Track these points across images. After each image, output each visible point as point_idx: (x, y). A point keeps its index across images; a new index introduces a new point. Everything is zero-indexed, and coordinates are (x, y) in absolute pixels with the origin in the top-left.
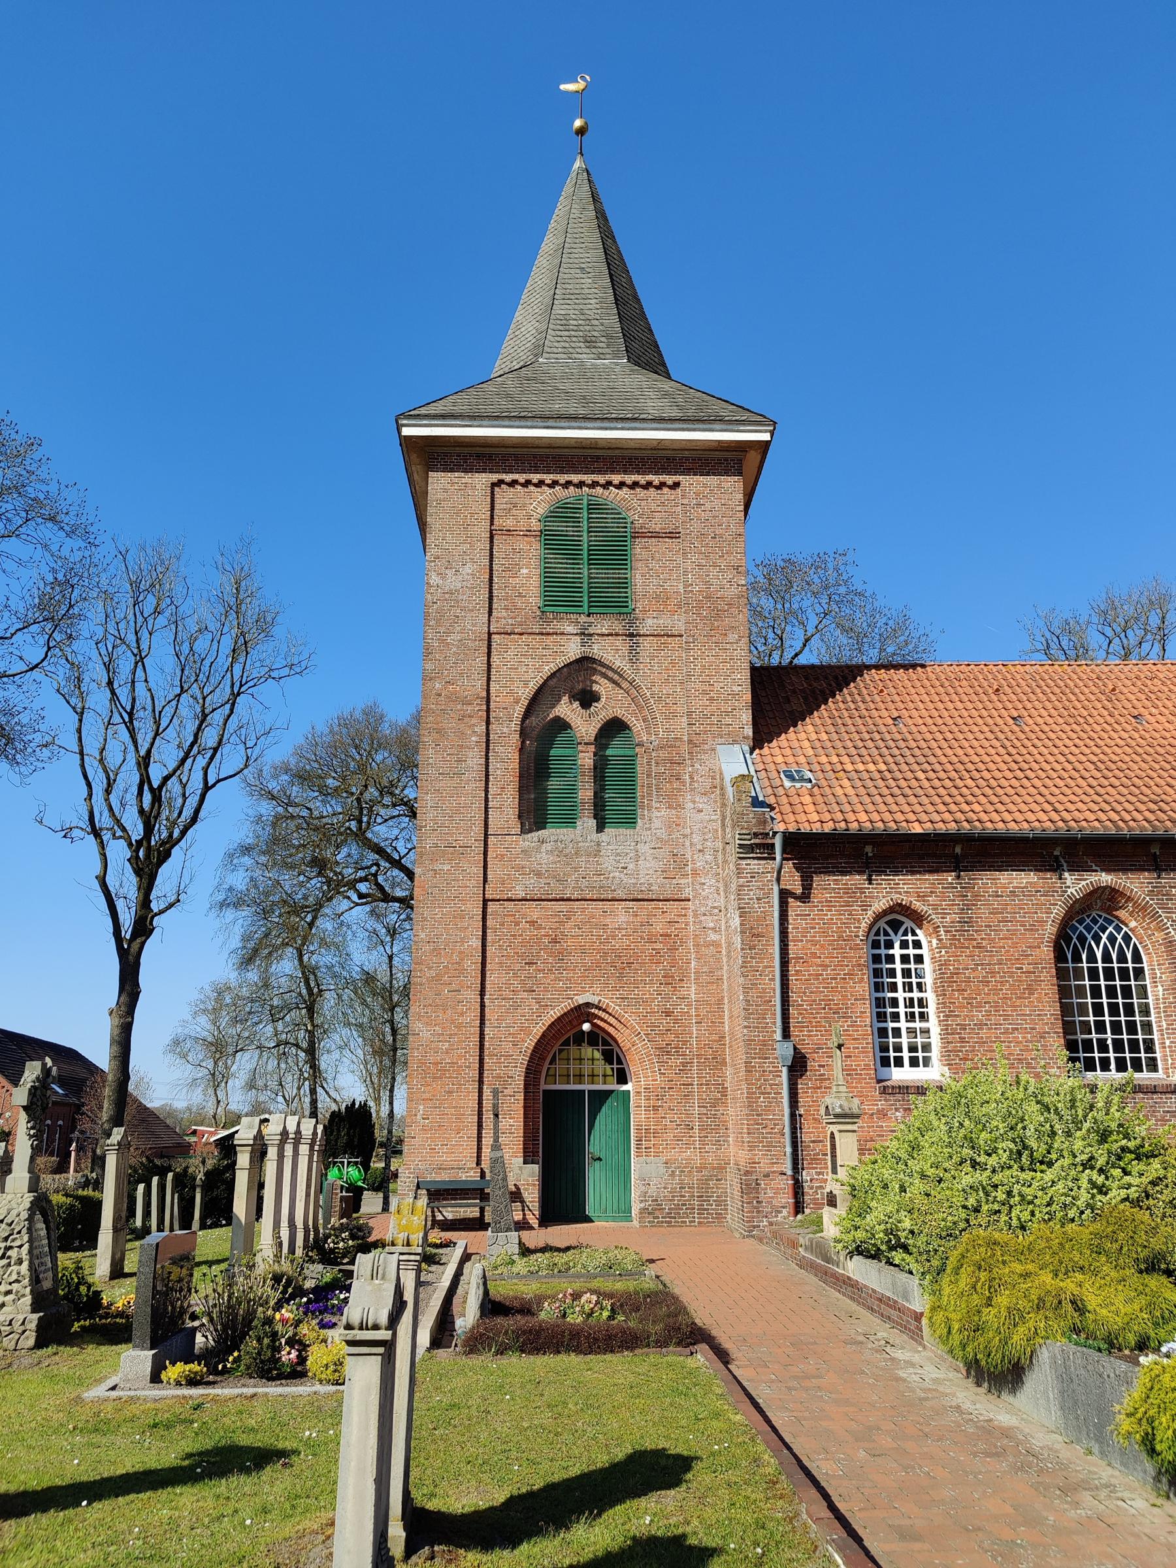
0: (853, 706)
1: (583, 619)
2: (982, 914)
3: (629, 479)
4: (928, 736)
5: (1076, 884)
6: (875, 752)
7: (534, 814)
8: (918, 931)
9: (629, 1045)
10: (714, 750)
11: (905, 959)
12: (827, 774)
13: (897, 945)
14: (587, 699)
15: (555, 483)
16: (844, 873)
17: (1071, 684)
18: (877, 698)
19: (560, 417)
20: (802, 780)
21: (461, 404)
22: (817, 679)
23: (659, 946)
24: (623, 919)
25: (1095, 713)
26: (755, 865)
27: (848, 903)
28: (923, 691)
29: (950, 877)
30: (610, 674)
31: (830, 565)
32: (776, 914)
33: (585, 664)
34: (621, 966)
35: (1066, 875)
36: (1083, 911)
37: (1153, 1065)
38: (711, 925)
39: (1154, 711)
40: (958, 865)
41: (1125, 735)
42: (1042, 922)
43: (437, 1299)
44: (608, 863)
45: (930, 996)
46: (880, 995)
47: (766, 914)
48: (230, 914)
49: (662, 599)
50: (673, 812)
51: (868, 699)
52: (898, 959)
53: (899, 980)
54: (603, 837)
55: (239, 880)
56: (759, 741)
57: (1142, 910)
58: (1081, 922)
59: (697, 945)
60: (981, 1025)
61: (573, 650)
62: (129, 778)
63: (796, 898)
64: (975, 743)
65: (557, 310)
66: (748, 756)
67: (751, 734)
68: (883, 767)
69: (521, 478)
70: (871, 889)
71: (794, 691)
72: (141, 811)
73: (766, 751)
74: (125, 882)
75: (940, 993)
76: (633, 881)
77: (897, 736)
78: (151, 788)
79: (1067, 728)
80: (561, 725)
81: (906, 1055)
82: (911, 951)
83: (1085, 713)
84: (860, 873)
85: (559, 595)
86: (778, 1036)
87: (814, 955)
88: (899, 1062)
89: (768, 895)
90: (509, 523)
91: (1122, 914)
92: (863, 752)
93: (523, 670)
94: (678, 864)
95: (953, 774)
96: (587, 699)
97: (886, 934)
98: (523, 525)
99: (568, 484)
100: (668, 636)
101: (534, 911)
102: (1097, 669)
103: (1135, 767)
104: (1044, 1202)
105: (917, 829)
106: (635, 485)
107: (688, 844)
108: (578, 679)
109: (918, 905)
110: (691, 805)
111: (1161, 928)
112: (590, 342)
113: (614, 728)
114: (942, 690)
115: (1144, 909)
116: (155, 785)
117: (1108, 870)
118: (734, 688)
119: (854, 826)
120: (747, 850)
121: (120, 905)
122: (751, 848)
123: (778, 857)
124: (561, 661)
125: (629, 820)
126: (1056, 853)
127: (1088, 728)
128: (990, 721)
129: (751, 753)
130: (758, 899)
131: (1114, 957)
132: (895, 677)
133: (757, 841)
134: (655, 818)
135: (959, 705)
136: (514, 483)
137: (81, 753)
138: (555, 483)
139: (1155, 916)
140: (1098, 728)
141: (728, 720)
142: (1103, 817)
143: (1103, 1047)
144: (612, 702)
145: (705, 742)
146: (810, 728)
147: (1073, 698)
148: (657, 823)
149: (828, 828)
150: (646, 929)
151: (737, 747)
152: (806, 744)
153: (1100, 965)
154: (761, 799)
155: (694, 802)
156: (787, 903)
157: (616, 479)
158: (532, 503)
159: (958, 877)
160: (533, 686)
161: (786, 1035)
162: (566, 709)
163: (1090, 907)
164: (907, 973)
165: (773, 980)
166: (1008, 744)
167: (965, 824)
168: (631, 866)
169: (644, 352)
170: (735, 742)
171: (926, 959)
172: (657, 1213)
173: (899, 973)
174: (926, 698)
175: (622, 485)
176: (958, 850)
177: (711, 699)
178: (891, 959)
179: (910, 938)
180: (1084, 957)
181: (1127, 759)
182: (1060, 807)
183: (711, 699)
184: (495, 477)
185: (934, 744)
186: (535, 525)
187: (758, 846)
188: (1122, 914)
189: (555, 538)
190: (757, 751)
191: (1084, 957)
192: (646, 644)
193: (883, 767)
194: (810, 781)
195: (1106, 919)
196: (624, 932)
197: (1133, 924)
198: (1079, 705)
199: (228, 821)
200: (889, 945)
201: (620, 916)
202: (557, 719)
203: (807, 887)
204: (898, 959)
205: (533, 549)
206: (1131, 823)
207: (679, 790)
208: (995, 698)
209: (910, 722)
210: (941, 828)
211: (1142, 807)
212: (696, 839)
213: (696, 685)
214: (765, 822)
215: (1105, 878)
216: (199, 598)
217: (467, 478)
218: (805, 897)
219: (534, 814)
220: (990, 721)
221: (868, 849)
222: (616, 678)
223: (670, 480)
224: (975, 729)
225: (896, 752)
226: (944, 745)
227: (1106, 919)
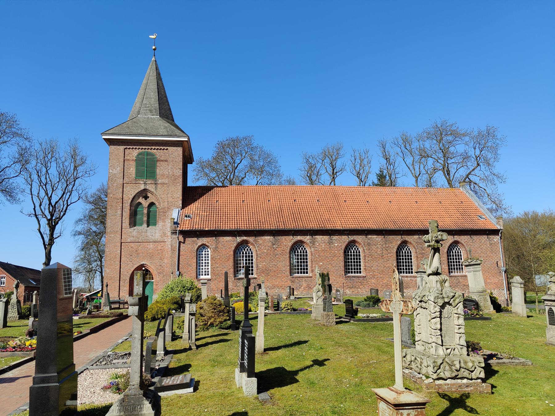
1: (145, 180)
2: (220, 246)
3: (156, 148)
5: (239, 239)
7: (133, 223)
11: (205, 254)
12: (198, 215)
14: (146, 198)
15: (139, 149)
19: (139, 135)
21: (116, 130)
26: (174, 236)
27: (193, 243)
29: (214, 238)
33: (145, 190)
34: (151, 256)
37: (307, 273)
43: (179, 360)
44: (149, 234)
48: (77, 237)
49: (163, 175)
54: (148, 228)
55: (80, 228)
56: (183, 207)
57: (252, 244)
61: (142, 187)
62: (46, 201)
65: (144, 102)
69: (131, 147)
72: (50, 212)
74: (46, 230)
78: (52, 206)
80: (140, 204)
81: (204, 273)
85: (139, 175)
88: (202, 275)
90: (128, 158)
93: (131, 192)
96: (146, 198)
98: (132, 158)
99: (142, 149)
101: (132, 245)
106: (158, 149)
108: (144, 194)
109: (207, 244)
111: (255, 248)
112: (151, 111)
113: (152, 204)
116: (53, 205)
120: (173, 233)
121: (45, 236)
122: (173, 233)
124: (140, 190)
125: (155, 224)
134: (160, 224)
136: (129, 148)
137: (32, 194)
138: (139, 149)
139: (254, 245)
143: (403, 269)
144: (151, 199)
157: (153, 147)
158: (134, 153)
160: (133, 195)
161: (178, 270)
162: (141, 200)
164: (205, 257)
169: (165, 113)
175: (154, 149)
178: (202, 254)
184: (125, 147)
186: (135, 158)
187: (174, 233)
189: (139, 161)
192: (159, 186)
199: (76, 212)
200: (202, 252)
201: (151, 246)
202: (139, 202)
203: (184, 241)
205: (134, 164)
210: (394, 228)
213: (169, 195)
215: (245, 238)
216: (63, 152)
217: (119, 147)
218: (184, 243)
219: (133, 223)
222: (152, 193)
223: (166, 148)
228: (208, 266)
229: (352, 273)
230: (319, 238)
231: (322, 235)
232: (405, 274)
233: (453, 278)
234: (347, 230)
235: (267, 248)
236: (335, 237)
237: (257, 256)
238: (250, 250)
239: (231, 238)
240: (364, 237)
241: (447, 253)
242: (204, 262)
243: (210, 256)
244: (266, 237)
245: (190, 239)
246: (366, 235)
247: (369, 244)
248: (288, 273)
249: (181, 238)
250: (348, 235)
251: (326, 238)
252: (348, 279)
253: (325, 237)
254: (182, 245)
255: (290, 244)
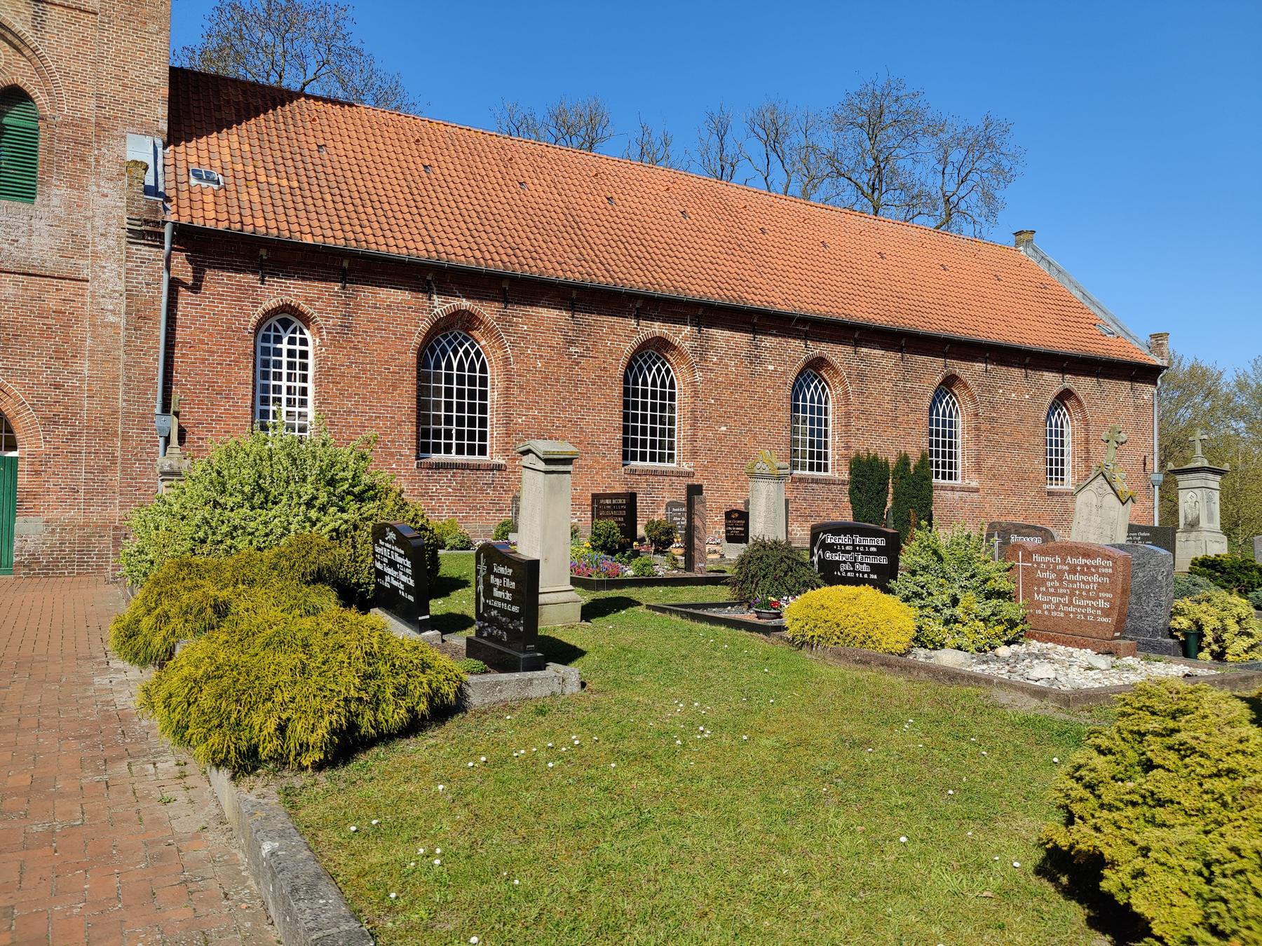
0: (283, 127)
2: (361, 321)
4: (346, 167)
5: (441, 305)
6: (292, 170)
8: (305, 331)
9: (13, 414)
10: (124, 137)
12: (231, 177)
13: (285, 340)
16: (238, 271)
17: (480, 148)
18: (308, 125)
20: (209, 180)
22: (254, 96)
23: (50, 321)
24: (11, 291)
25: (491, 174)
26: (145, 252)
27: (233, 300)
28: (352, 128)
29: (337, 287)
30: (10, 37)
31: (331, 17)
32: (164, 300)
35: (435, 297)
36: (446, 329)
37: (483, 451)
38: (111, 307)
39: (536, 181)
40: (345, 277)
41: (508, 195)
42: (411, 333)
45: (310, 386)
46: (266, 382)
47: (153, 300)
50: (75, 192)
51: (300, 123)
52: (285, 353)
53: (284, 371)
57: (490, 331)
58: (445, 337)
59: (93, 325)
60: (349, 412)
63: (187, 288)
64: (386, 180)
66: (160, 149)
67: (166, 129)
68: (295, 184)
70: (263, 289)
71: (228, 102)
73: (181, 149)
75: (318, 384)
76: (24, 255)
77: (318, 161)
79: (466, 182)
82: (298, 347)
83: (484, 173)
84: (253, 273)
86: (158, 410)
87: (202, 342)
89: (159, 281)
91: (476, 334)
92: (281, 168)
94: (78, 244)
95: (358, 202)
97: (276, 330)
100: (80, 10)
102: (503, 141)
103: (508, 220)
104: (263, 533)
105: (308, 240)
107: (89, 226)
109: (305, 308)
110: (94, 188)
111: (502, 347)
114: (370, 131)
115: (491, 331)
117: (468, 298)
118: (151, 80)
119: (249, 229)
122: (142, 235)
123: (167, 246)
126: (429, 278)
127: (482, 185)
128: (405, 165)
129: (164, 148)
130: (147, 284)
131: (455, 365)
132: (331, 111)
133: (148, 228)
134: (55, 194)
135: (382, 147)
139: (499, 337)
140: (490, 186)
141: (142, 111)
142: (469, 253)
143: (448, 435)
145: (114, 128)
146: (235, 138)
147: (478, 159)
148: (55, 201)
149: (222, 226)
150: (37, 304)
151: (149, 140)
152: (226, 150)
153: (455, 372)
154: (161, 189)
155: (99, 186)
156: (177, 291)
159: (344, 288)
161: (166, 408)
163: (452, 326)
164: (291, 365)
165: (157, 360)
166: (413, 185)
167: (353, 242)
168: (23, 240)
170: (147, 134)
171: (311, 355)
172: (34, 566)
173: (285, 365)
174: (353, 134)
176: (345, 264)
177: (125, 86)
178: (278, 352)
179: (298, 336)
180: (443, 365)
181: (504, 213)
182: (437, 241)
183: (125, 86)
185: (349, 174)
187: (146, 232)
188: (476, 334)
190: (172, 147)
191: (443, 365)
193: (295, 184)
194: (218, 183)
195: (464, 337)
196: (11, 304)
197: (483, 343)
198: (481, 166)
200: (278, 339)
204: (285, 353)
206: (490, 262)
207: (83, 171)
208: (414, 146)
209: (333, 151)
210: (331, 242)
211: (501, 251)
212: (99, 222)
213: (106, 68)
214: (157, 211)
215: (465, 304)
218: (196, 288)
220: (405, 165)
221: (263, 252)
224: (390, 168)
225: (312, 174)
226: (358, 176)
227: (464, 337)
228: (303, 403)
229: (643, 459)
230: (721, 336)
231: (731, 329)
232: (807, 472)
233: (1056, 498)
234: (804, 320)
235: (546, 352)
236: (768, 342)
237: (509, 379)
238: (478, 354)
239: (407, 295)
240: (849, 349)
241: (626, 381)
242: (284, 383)
243: (311, 361)
244: (544, 312)
245: (225, 276)
246: (857, 344)
247: (861, 376)
248: (409, 450)
249: (182, 268)
250: (805, 337)
251: (740, 339)
252: (801, 486)
253: (737, 335)
254: (184, 297)
255: (628, 348)
